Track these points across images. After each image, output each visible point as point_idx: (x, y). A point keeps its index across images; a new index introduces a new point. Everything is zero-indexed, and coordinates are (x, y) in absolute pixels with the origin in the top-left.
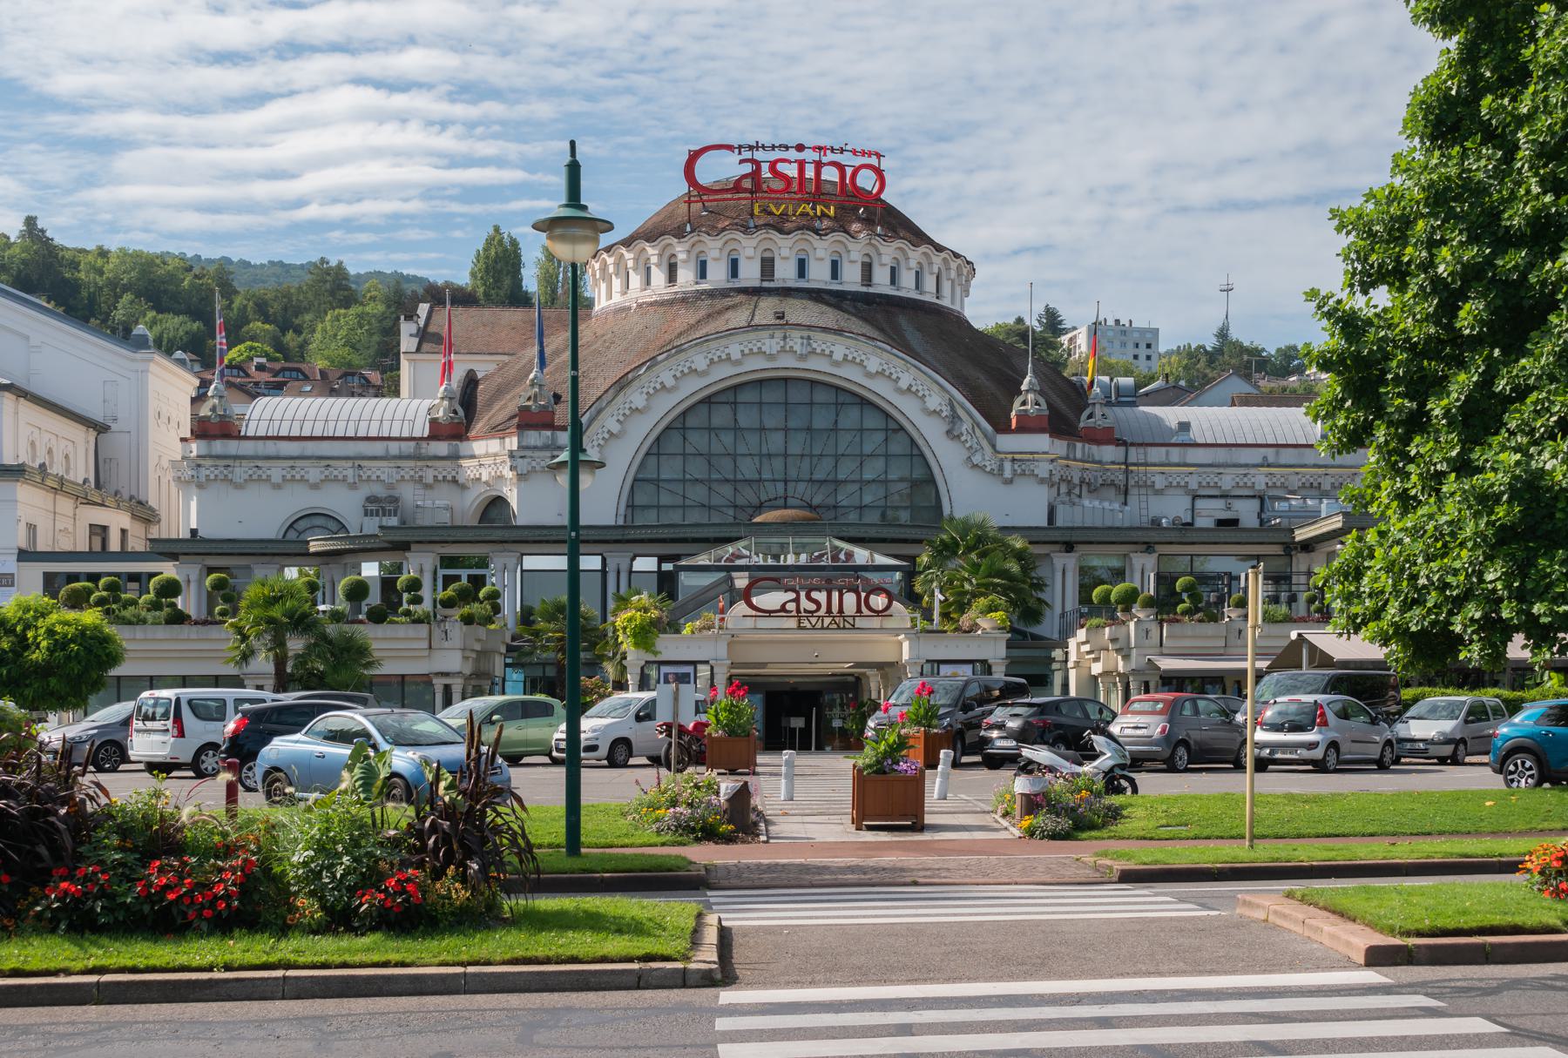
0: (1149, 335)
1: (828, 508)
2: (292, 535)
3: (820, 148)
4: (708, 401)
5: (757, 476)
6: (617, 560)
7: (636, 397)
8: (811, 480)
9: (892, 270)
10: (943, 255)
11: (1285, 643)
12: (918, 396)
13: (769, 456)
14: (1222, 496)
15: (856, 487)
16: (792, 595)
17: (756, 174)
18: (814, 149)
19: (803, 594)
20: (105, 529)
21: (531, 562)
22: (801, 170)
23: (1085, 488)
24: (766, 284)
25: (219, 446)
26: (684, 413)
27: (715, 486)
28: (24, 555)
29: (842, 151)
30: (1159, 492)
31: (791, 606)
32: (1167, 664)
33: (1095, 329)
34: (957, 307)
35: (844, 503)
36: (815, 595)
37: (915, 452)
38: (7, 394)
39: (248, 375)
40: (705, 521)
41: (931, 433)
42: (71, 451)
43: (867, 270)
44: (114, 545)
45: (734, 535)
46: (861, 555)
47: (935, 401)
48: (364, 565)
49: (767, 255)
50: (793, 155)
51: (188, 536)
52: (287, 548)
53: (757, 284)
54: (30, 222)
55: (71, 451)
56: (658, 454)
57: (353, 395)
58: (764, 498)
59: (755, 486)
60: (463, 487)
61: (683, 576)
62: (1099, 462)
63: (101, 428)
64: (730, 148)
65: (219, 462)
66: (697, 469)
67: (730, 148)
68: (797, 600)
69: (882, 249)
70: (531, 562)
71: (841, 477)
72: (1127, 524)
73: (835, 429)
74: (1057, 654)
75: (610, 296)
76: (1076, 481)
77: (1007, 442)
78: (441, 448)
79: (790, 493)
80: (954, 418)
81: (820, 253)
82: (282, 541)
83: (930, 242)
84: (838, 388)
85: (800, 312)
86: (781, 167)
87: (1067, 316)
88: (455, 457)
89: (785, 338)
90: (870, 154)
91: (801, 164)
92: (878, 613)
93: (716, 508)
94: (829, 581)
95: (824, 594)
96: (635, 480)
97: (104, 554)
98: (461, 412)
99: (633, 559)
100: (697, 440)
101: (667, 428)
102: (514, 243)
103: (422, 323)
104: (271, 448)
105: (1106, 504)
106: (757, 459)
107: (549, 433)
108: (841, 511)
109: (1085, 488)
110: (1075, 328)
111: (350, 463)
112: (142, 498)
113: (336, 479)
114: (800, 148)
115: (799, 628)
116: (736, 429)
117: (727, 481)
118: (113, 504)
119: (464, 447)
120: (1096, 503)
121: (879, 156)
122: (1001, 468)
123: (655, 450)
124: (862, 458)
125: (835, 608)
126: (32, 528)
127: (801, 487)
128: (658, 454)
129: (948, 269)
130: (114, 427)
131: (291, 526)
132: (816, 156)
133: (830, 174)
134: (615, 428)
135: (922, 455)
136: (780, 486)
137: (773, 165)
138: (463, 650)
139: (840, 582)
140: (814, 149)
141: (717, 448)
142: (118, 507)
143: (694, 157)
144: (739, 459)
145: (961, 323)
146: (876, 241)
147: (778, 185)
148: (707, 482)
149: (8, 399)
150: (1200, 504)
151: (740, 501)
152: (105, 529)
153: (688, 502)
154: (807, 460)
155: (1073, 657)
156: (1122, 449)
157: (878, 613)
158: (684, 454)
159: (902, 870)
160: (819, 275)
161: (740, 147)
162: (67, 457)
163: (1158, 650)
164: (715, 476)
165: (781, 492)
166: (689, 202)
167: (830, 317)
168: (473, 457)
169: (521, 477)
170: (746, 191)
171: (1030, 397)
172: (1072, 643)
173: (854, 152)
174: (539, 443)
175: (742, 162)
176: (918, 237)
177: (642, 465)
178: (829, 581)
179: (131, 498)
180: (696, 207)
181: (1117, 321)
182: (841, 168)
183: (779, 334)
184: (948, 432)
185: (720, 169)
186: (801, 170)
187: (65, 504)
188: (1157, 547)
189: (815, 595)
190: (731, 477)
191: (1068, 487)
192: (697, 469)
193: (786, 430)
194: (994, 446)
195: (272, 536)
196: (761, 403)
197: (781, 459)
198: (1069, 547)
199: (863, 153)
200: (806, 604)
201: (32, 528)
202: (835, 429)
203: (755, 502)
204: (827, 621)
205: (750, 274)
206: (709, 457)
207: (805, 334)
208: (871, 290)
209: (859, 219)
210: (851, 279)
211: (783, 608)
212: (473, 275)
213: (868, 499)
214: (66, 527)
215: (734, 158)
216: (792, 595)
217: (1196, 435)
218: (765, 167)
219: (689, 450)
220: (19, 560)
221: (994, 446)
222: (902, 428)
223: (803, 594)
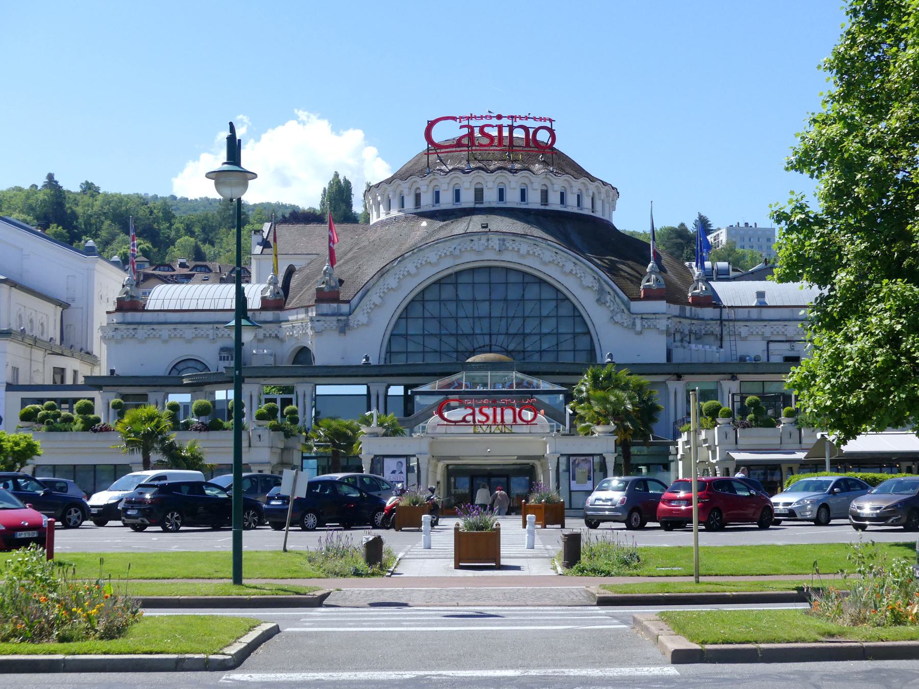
0: (768, 233)
1: (519, 352)
2: (175, 373)
3: (512, 117)
4: (438, 282)
5: (471, 332)
7: (391, 281)
8: (507, 334)
9: (562, 195)
10: (596, 184)
11: (815, 441)
12: (576, 276)
13: (480, 318)
14: (787, 341)
15: (538, 337)
16: (470, 411)
17: (471, 135)
18: (508, 117)
19: (477, 410)
20: (63, 370)
21: (321, 390)
22: (500, 132)
23: (693, 337)
24: (478, 206)
25: (130, 316)
26: (423, 291)
27: (444, 338)
28: (10, 387)
29: (527, 118)
30: (744, 339)
31: (470, 418)
32: (738, 456)
33: (730, 229)
34: (606, 218)
35: (528, 349)
36: (485, 410)
37: (404, 315)
38: (4, 285)
39: (174, 270)
41: (586, 300)
42: (47, 319)
43: (545, 194)
44: (69, 381)
45: (453, 371)
46: (544, 385)
47: (589, 281)
48: (217, 392)
49: (479, 186)
50: (495, 122)
51: (109, 374)
52: (171, 381)
53: (471, 205)
54: (50, 177)
55: (47, 319)
56: (407, 318)
57: (176, 283)
58: (476, 346)
60: (282, 341)
61: (418, 398)
62: (703, 319)
63: (64, 305)
64: (454, 118)
65: (129, 326)
66: (432, 327)
67: (454, 118)
68: (473, 414)
69: (554, 181)
70: (321, 390)
71: (527, 331)
72: (722, 360)
73: (523, 299)
74: (672, 448)
75: (379, 216)
76: (686, 332)
77: (636, 306)
78: (269, 315)
79: (493, 342)
80: (601, 291)
81: (513, 185)
82: (168, 377)
83: (587, 175)
84: (524, 274)
85: (499, 223)
86: (486, 130)
87: (714, 223)
88: (278, 322)
89: (488, 240)
90: (545, 120)
91: (500, 128)
93: (446, 353)
94: (494, 401)
95: (491, 410)
96: (392, 335)
97: (63, 387)
98: (282, 293)
100: (432, 309)
101: (413, 301)
102: (348, 183)
103: (265, 236)
104: (162, 317)
105: (707, 347)
106: (471, 320)
107: (335, 305)
108: (527, 354)
109: (693, 337)
110: (719, 229)
111: (211, 326)
112: (89, 350)
113: (202, 336)
114: (499, 117)
115: (475, 433)
116: (457, 300)
117: (452, 335)
118: (70, 354)
119: (282, 315)
120: (700, 346)
121: (551, 121)
122: (634, 324)
124: (541, 318)
126: (16, 370)
127: (501, 338)
128: (407, 318)
129: (600, 193)
130: (72, 304)
131: (174, 367)
132: (509, 122)
133: (519, 134)
134: (378, 301)
135: (581, 316)
136: (487, 338)
137: (482, 129)
138: (272, 447)
140: (508, 117)
141: (445, 313)
142: (73, 356)
143: (431, 124)
144: (459, 320)
145: (608, 227)
146: (551, 177)
147: (486, 141)
148: (439, 336)
149: (5, 287)
150: (772, 346)
151: (461, 348)
152: (63, 370)
153: (426, 349)
154: (504, 321)
155: (681, 452)
156: (718, 310)
158: (423, 318)
159: (63, 554)
160: (513, 199)
161: (461, 118)
162: (42, 324)
163: (734, 446)
164: (443, 332)
165: (487, 342)
166: (428, 154)
167: (518, 227)
168: (288, 321)
169: (318, 333)
170: (463, 146)
171: (653, 276)
172: (680, 441)
173: (535, 119)
174: (329, 312)
175: (461, 127)
176: (579, 172)
177: (396, 324)
178: (494, 401)
179: (81, 350)
180: (433, 157)
181: (746, 224)
182: (526, 129)
183: (484, 238)
184: (598, 300)
185: (445, 133)
186: (500, 132)
187: (38, 354)
188: (739, 376)
189: (485, 410)
190: (454, 332)
191: (677, 337)
192: (432, 327)
193: (490, 301)
194: (629, 310)
195: (161, 374)
196: (473, 283)
197: (487, 320)
198: (679, 377)
199: (541, 119)
200: (479, 417)
201: (16, 370)
202: (523, 299)
203: (471, 349)
204: (493, 428)
205: (467, 199)
206: (440, 319)
207: (502, 237)
208: (547, 208)
209: (540, 162)
210: (534, 201)
211: (464, 420)
212: (323, 204)
214: (40, 369)
215: (457, 124)
216: (470, 411)
217: (769, 301)
218: (477, 130)
220: (7, 390)
221: (629, 310)
222: (567, 299)
223: (477, 410)
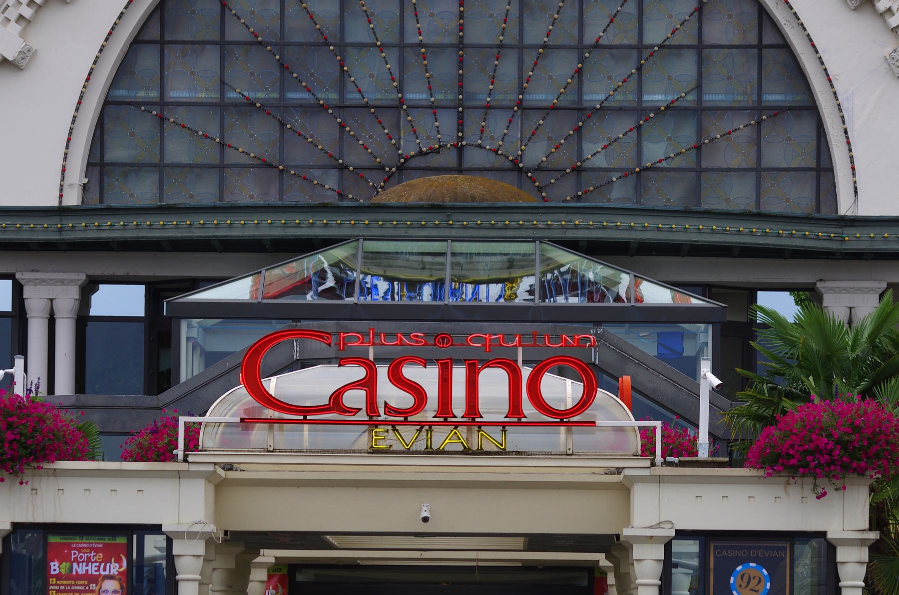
6: (46, 292)
15: (628, 123)
16: (358, 373)
19: (382, 371)
27: (296, 121)
31: (356, 398)
35: (600, 161)
36: (410, 372)
40: (274, 200)
48: (791, 320)
56: (162, 43)
59: (387, 118)
68: (369, 384)
79: (472, 136)
92: (562, 418)
96: (108, 103)
99: (89, 288)
106: (392, 56)
123: (154, 33)
125: (459, 407)
127: (498, 125)
128: (162, 43)
135: (785, 46)
136: (447, 122)
139: (391, 347)
148: (277, 111)
151: (354, 158)
157: (562, 418)
164: (294, 96)
177: (124, 70)
189: (410, 372)
192: (250, 83)
200: (389, 393)
211: (336, 401)
213: (655, 151)
216: (358, 373)
219: (235, 32)
223: (382, 371)
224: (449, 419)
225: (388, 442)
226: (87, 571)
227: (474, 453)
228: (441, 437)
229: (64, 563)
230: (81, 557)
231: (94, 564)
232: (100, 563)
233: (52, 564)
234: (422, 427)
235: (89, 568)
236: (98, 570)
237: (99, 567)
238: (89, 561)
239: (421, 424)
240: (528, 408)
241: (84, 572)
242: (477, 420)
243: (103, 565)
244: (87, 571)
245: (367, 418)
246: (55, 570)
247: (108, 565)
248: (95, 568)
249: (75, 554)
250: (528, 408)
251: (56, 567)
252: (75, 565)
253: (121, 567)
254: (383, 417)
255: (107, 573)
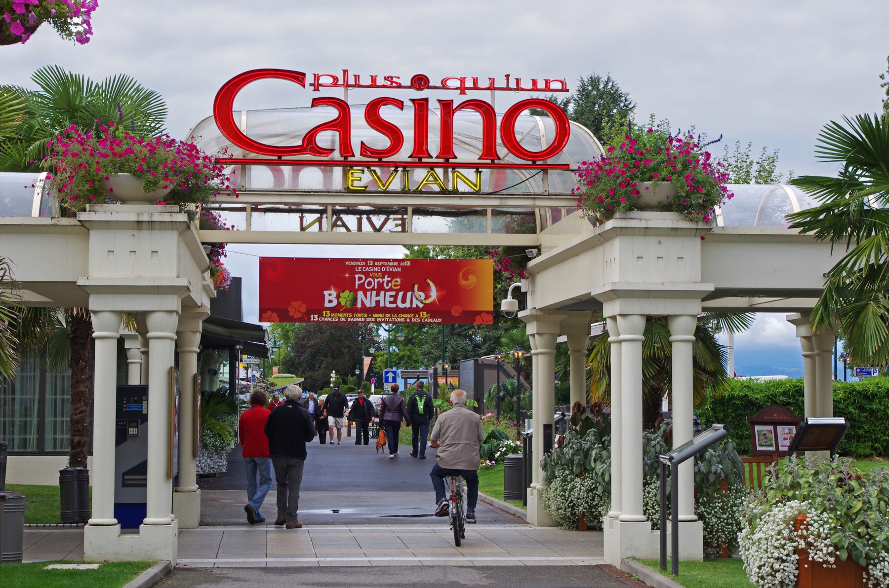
31: (325, 139)
125: (434, 144)
224: (424, 160)
225: (362, 183)
226: (378, 302)
227: (450, 193)
228: (420, 174)
229: (347, 292)
230: (370, 283)
231: (388, 294)
232: (398, 292)
233: (326, 293)
234: (397, 167)
235: (381, 298)
236: (395, 302)
237: (395, 297)
238: (380, 288)
239: (396, 165)
240: (502, 151)
241: (374, 304)
242: (451, 161)
243: (401, 294)
244: (378, 302)
245: (342, 159)
246: (330, 301)
247: (409, 294)
248: (388, 299)
249: (360, 279)
250: (502, 151)
251: (333, 297)
252: (360, 294)
253: (427, 297)
254: (358, 157)
255: (407, 305)
